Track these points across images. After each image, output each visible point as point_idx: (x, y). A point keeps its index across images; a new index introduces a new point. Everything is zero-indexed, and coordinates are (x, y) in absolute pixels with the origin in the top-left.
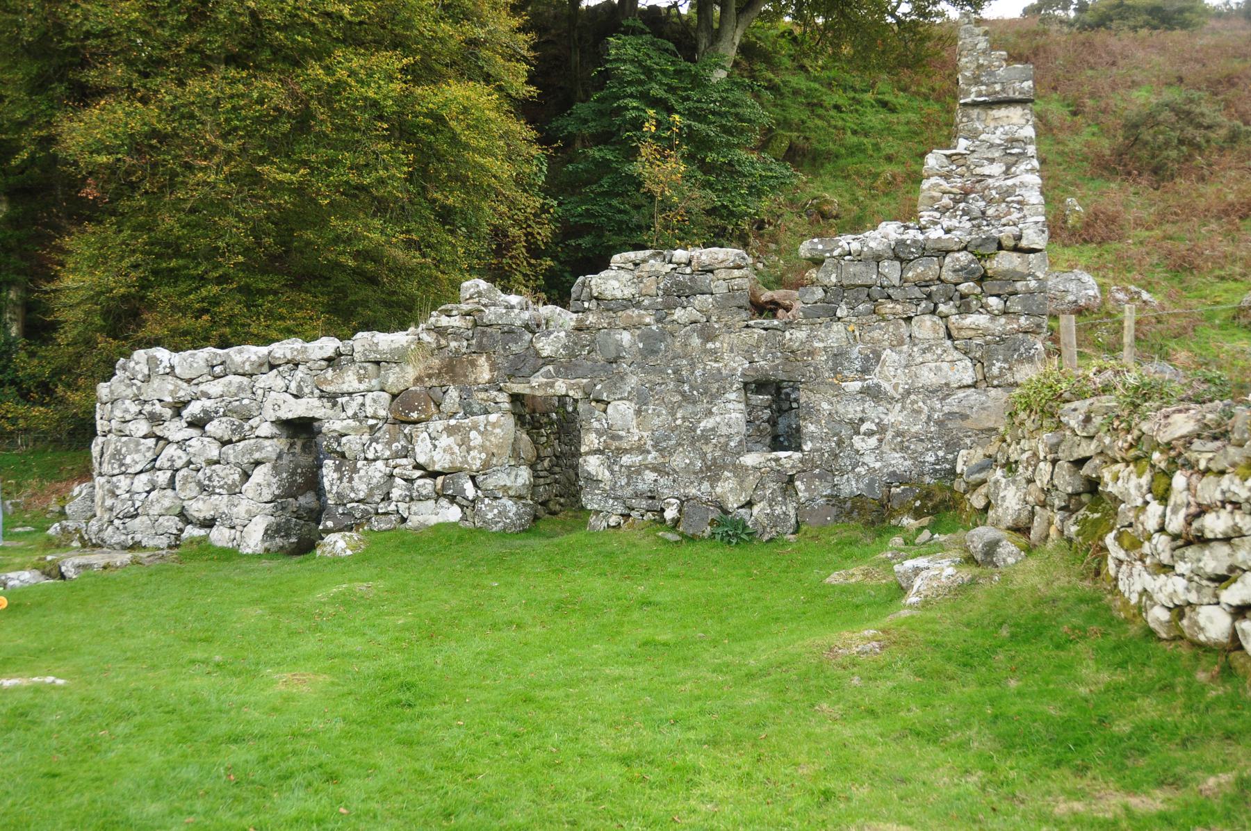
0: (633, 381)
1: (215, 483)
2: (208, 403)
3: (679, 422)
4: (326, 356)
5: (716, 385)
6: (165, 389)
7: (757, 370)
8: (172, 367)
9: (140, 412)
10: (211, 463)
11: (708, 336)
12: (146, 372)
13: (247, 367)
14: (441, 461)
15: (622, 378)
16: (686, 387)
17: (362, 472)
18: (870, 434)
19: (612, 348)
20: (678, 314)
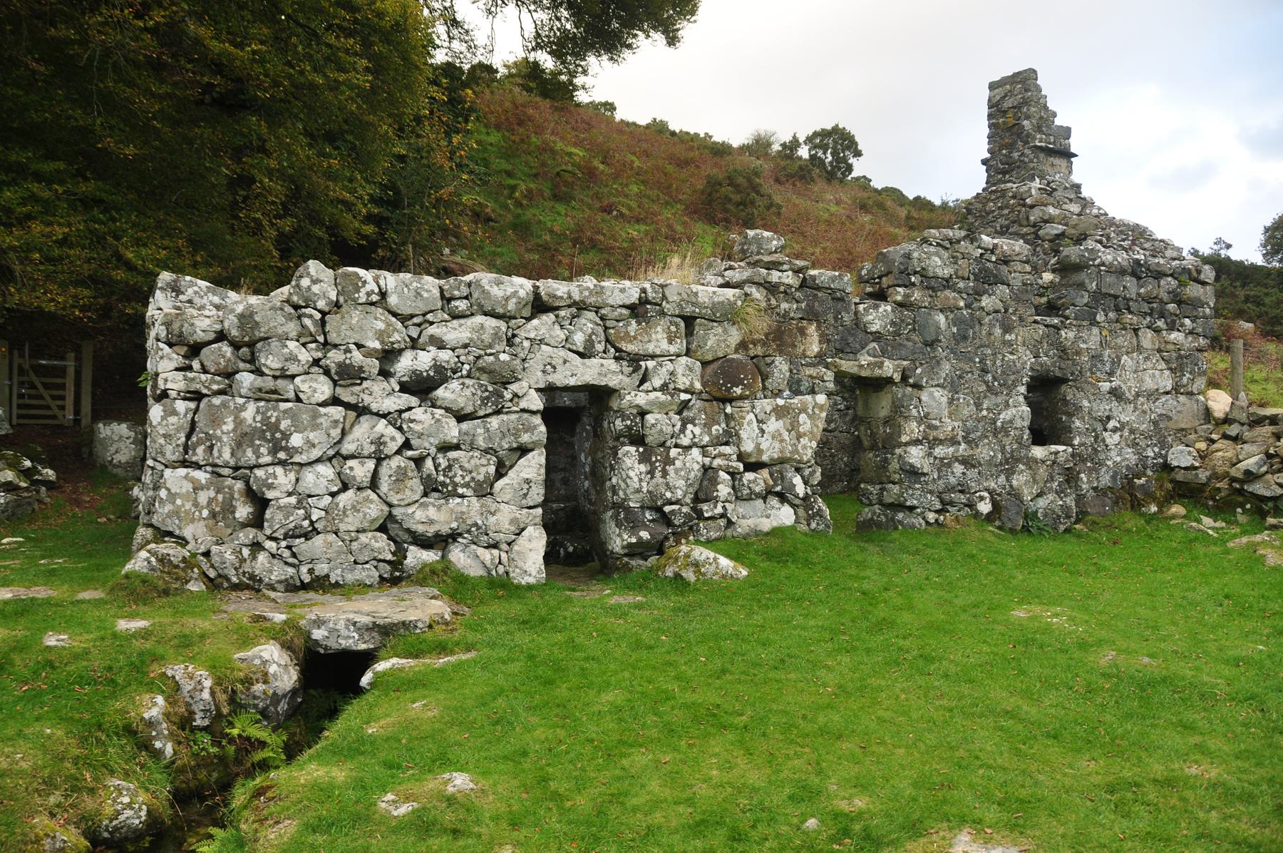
0: (946, 367)
1: (458, 479)
2: (445, 356)
3: (985, 413)
4: (628, 302)
5: (1012, 377)
6: (364, 330)
8: (383, 295)
9: (316, 362)
10: (445, 448)
11: (1007, 329)
12: (333, 295)
13: (511, 306)
14: (770, 450)
15: (938, 363)
16: (989, 377)
17: (678, 464)
18: (1115, 430)
19: (932, 329)
20: (986, 301)
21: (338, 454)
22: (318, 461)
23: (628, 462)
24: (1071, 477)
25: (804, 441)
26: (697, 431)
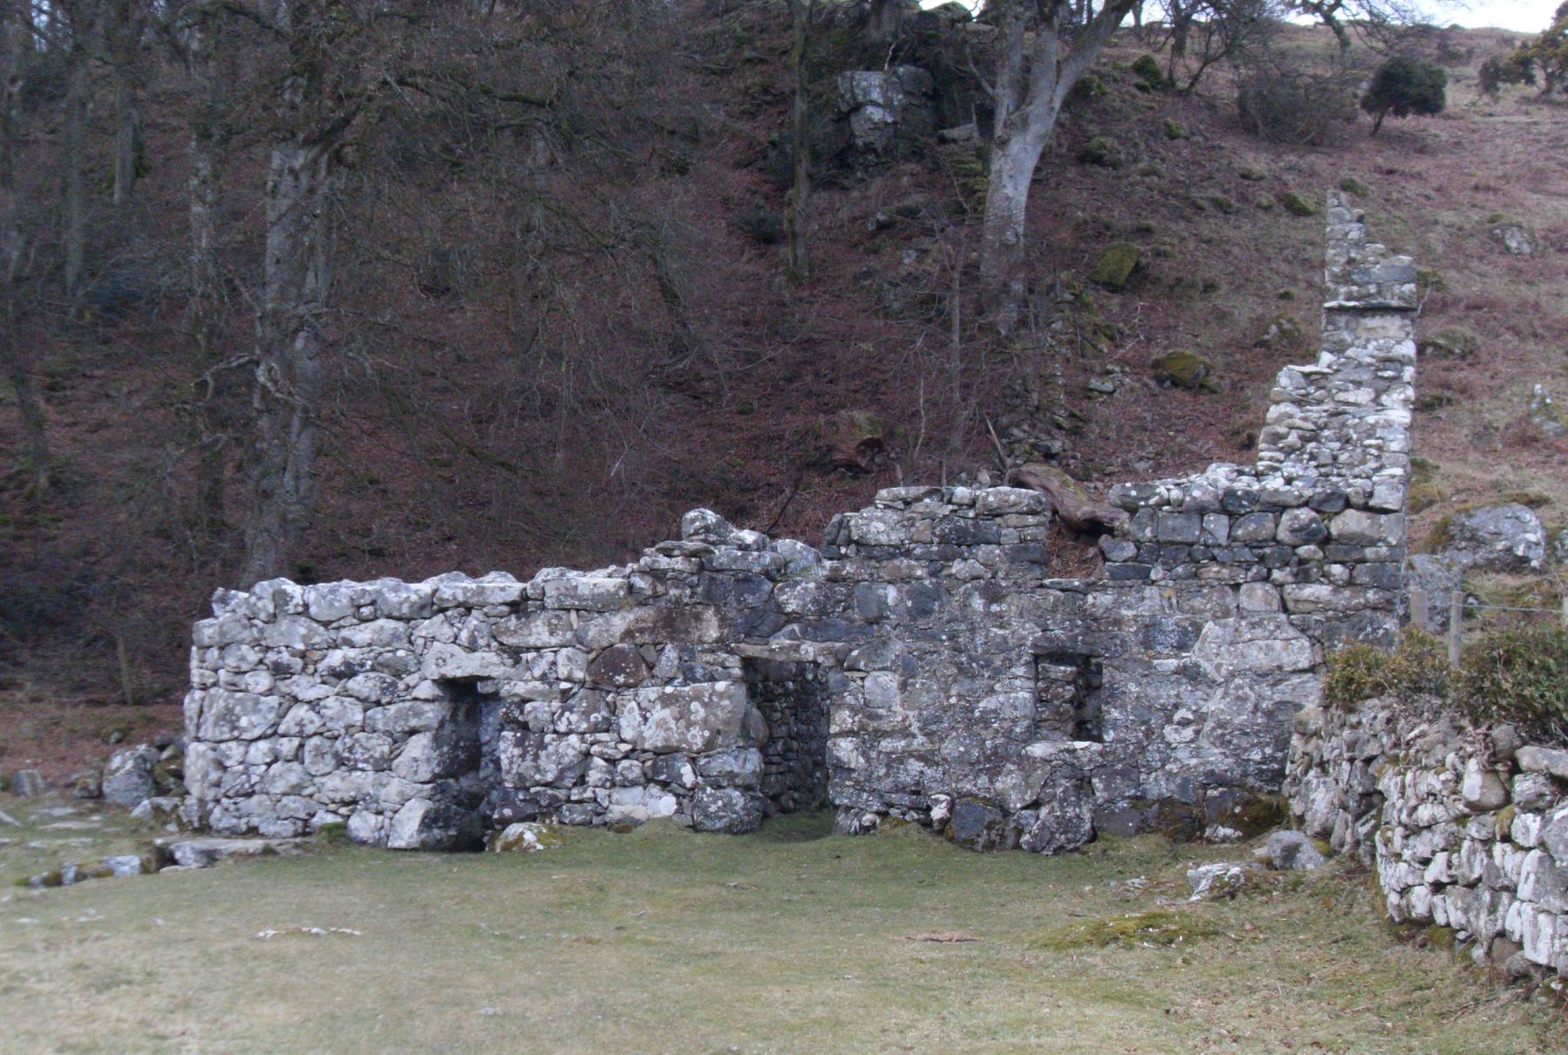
0: (897, 647)
1: (358, 756)
2: (351, 653)
3: (953, 700)
4: (509, 599)
7: (1050, 640)
8: (306, 606)
9: (261, 662)
12: (271, 609)
14: (653, 738)
17: (551, 749)
18: (1185, 723)
20: (957, 567)
21: (275, 733)
22: (259, 738)
23: (1323, 805)
24: (1083, 785)
25: (695, 731)
26: (574, 718)
